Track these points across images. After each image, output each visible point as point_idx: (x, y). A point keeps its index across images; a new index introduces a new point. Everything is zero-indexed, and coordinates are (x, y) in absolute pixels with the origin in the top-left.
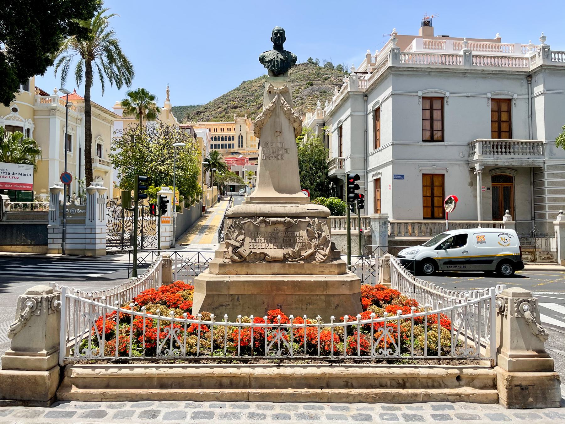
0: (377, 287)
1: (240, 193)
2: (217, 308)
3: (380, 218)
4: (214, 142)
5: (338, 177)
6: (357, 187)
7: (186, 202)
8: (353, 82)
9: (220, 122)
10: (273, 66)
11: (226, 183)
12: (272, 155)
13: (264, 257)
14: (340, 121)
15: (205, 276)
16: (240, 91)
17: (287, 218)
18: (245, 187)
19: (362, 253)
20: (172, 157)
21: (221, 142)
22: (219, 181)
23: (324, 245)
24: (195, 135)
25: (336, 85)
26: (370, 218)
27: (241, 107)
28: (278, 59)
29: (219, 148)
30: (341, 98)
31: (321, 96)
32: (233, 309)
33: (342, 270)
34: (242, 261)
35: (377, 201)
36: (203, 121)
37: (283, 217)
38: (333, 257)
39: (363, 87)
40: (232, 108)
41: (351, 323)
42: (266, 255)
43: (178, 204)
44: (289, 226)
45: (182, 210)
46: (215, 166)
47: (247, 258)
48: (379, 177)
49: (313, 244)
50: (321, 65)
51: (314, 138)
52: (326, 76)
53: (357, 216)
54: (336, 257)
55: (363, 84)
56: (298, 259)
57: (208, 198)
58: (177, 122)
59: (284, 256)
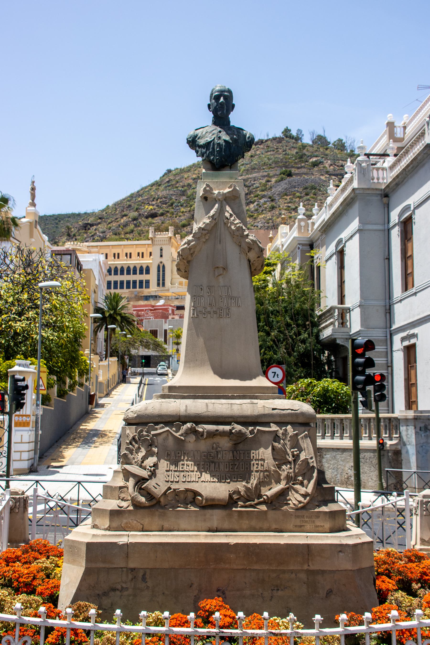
0: (409, 554)
1: (160, 369)
2: (105, 594)
3: (416, 419)
4: (113, 278)
5: (338, 342)
6: (370, 363)
7: (59, 386)
8: (363, 172)
9: (125, 242)
10: (212, 153)
11: (133, 352)
12: (209, 309)
13: (191, 497)
14: (340, 241)
15: (85, 533)
16: (162, 188)
17: (236, 426)
18: (167, 358)
19: (385, 485)
20: (37, 307)
21: (125, 278)
22: (121, 349)
23: (303, 476)
24: (79, 266)
25: (334, 175)
26: (396, 419)
27: (162, 214)
28: (221, 142)
29: (122, 287)
30: (341, 200)
31: (307, 194)
32: (135, 596)
33: (338, 522)
34: (153, 506)
35: (410, 386)
36: (94, 240)
37: (229, 424)
38: (320, 498)
39: (381, 181)
40: (147, 217)
41: (353, 629)
42: (196, 493)
43: (45, 392)
44: (239, 440)
45: (53, 402)
46: (113, 320)
47: (162, 500)
48: (413, 341)
49: (284, 474)
50: (307, 140)
51: (294, 272)
52: (314, 159)
53: (348, 443)
54: (327, 498)
55: (381, 176)
56: (256, 501)
57: (101, 379)
58: (47, 244)
59: (230, 496)
